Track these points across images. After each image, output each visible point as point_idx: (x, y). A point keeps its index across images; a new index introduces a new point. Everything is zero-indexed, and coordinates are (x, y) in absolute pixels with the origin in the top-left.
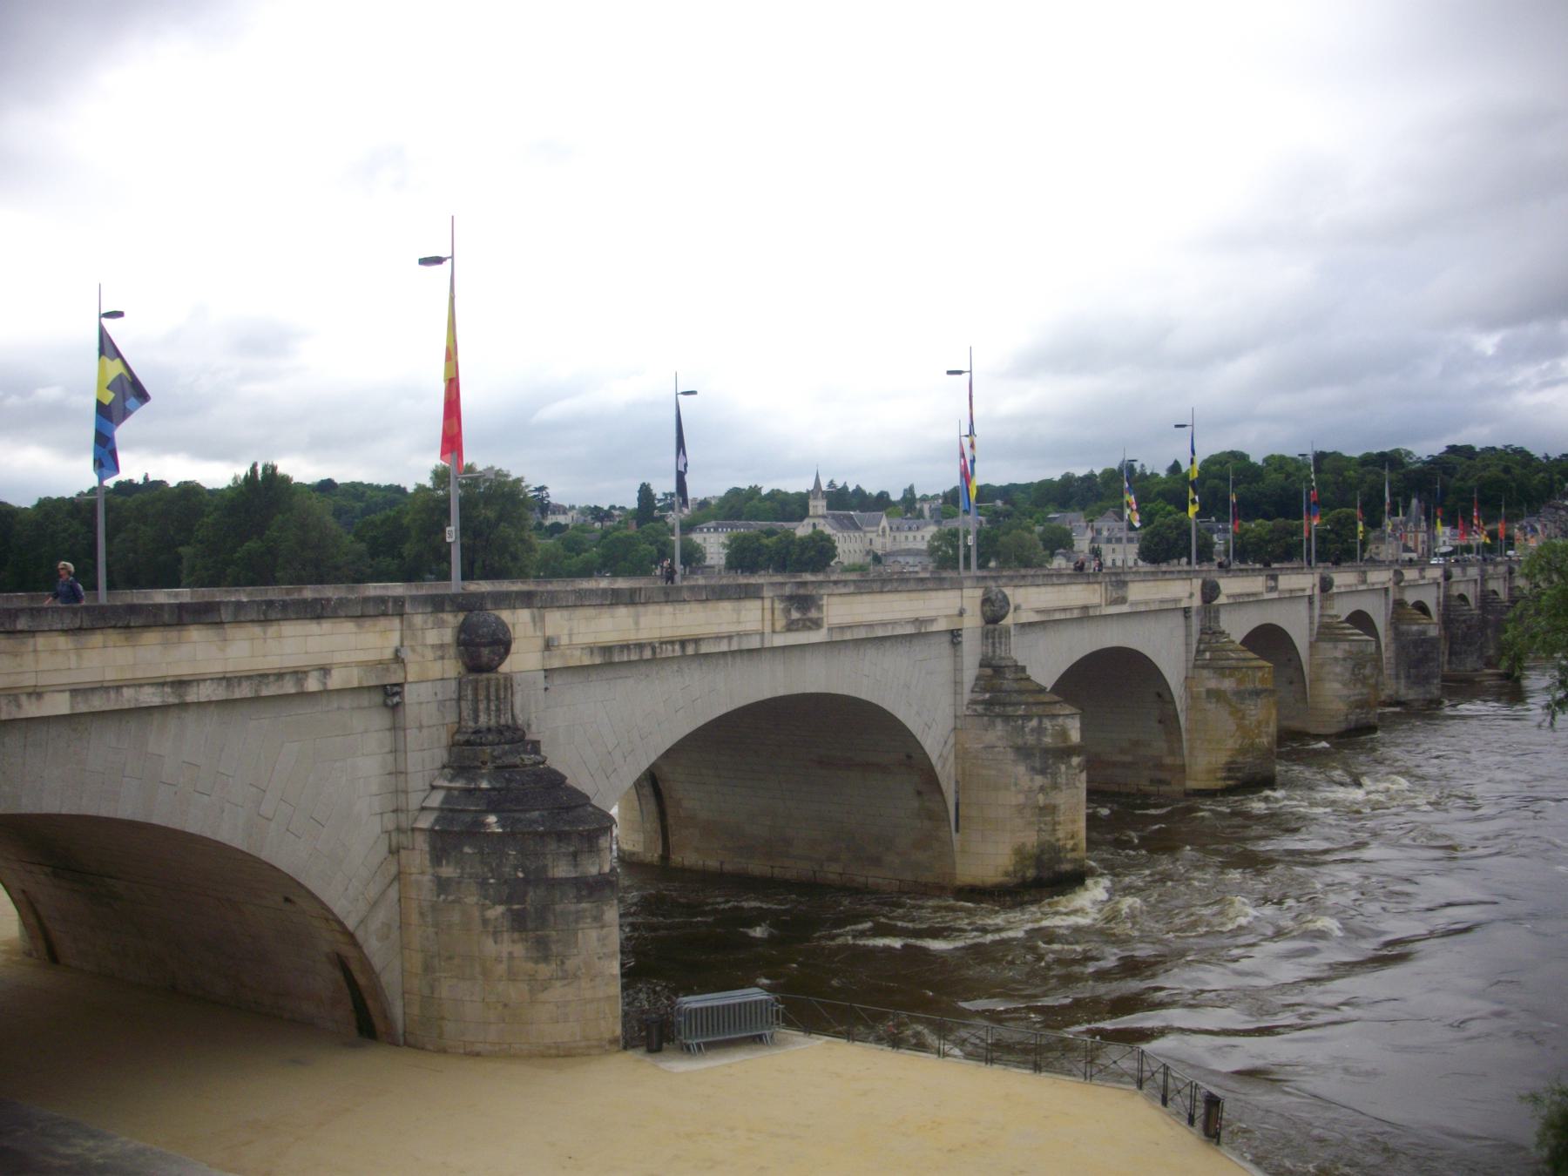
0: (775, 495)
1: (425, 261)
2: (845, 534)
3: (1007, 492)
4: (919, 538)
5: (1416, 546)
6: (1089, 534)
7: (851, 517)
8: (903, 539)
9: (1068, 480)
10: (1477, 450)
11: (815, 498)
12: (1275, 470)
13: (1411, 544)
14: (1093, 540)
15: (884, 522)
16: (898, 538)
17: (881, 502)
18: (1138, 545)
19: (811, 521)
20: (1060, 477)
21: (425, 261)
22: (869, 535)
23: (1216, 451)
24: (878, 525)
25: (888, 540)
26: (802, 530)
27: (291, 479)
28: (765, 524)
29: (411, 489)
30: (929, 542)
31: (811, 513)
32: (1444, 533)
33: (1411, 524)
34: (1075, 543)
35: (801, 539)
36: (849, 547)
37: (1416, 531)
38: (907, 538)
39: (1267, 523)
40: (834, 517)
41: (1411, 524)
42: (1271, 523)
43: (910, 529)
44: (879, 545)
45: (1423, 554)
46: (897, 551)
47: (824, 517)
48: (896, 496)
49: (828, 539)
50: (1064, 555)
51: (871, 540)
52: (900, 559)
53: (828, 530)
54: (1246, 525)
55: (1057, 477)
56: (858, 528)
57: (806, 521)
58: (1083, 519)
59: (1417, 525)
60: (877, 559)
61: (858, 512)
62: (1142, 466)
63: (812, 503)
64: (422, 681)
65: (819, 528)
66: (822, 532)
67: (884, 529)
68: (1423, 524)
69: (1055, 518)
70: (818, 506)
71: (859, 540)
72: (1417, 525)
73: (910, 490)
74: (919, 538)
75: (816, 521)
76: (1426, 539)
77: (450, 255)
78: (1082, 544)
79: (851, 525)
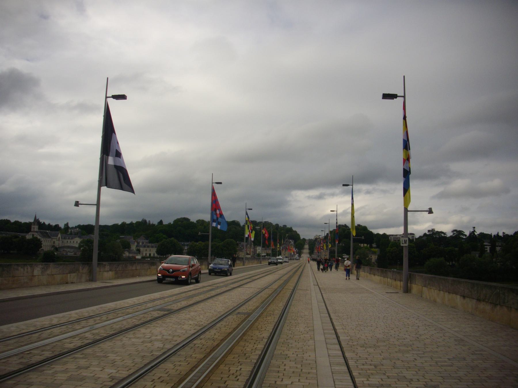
0: (17, 223)
1: (386, 96)
2: (45, 239)
3: (106, 227)
4: (75, 242)
5: (250, 253)
6: (136, 244)
7: (47, 233)
8: (66, 242)
9: (124, 224)
10: (513, 235)
11: (34, 225)
12: (200, 225)
13: (248, 252)
14: (137, 246)
15: (59, 236)
16: (64, 242)
17: (57, 228)
18: (156, 249)
19: (32, 233)
20: (121, 223)
21: (386, 96)
22: (54, 240)
23: (179, 217)
24: (57, 236)
25: (61, 242)
26: (29, 236)
27: (170, 223)
28: (13, 233)
29: (302, 238)
30: (79, 244)
31: (32, 230)
32: (259, 249)
33: (249, 245)
34: (131, 247)
35: (28, 240)
36: (46, 245)
37: (251, 248)
38: (67, 241)
39: (203, 243)
40: (41, 232)
41: (249, 245)
42: (204, 243)
43: (69, 239)
44: (57, 244)
45: (252, 256)
46: (64, 246)
47: (37, 232)
48: (62, 226)
49: (39, 240)
50: (128, 251)
51: (54, 242)
52: (65, 249)
53: (39, 237)
54: (195, 243)
55: (120, 223)
56: (49, 237)
57: (30, 233)
58: (132, 238)
59: (251, 246)
60: (57, 249)
61: (49, 231)
62: (149, 221)
63: (33, 226)
64: (315, 350)
65: (35, 236)
66: (37, 238)
67: (59, 238)
68: (253, 245)
69: (123, 238)
70: (35, 228)
71: (49, 241)
72: (251, 246)
73: (67, 224)
74: (75, 242)
75: (34, 233)
76: (253, 251)
77: (108, 99)
78: (134, 247)
79: (47, 236)
